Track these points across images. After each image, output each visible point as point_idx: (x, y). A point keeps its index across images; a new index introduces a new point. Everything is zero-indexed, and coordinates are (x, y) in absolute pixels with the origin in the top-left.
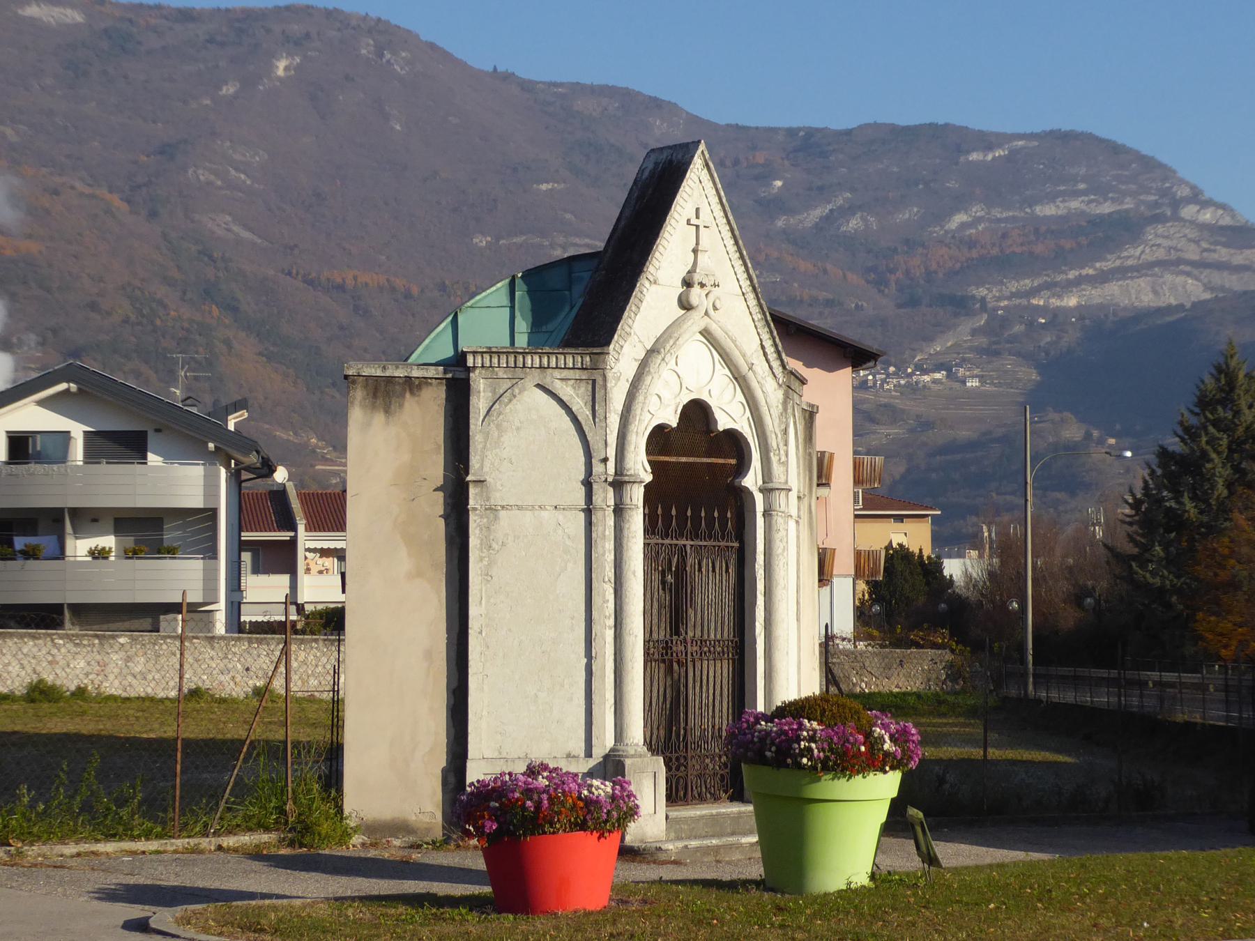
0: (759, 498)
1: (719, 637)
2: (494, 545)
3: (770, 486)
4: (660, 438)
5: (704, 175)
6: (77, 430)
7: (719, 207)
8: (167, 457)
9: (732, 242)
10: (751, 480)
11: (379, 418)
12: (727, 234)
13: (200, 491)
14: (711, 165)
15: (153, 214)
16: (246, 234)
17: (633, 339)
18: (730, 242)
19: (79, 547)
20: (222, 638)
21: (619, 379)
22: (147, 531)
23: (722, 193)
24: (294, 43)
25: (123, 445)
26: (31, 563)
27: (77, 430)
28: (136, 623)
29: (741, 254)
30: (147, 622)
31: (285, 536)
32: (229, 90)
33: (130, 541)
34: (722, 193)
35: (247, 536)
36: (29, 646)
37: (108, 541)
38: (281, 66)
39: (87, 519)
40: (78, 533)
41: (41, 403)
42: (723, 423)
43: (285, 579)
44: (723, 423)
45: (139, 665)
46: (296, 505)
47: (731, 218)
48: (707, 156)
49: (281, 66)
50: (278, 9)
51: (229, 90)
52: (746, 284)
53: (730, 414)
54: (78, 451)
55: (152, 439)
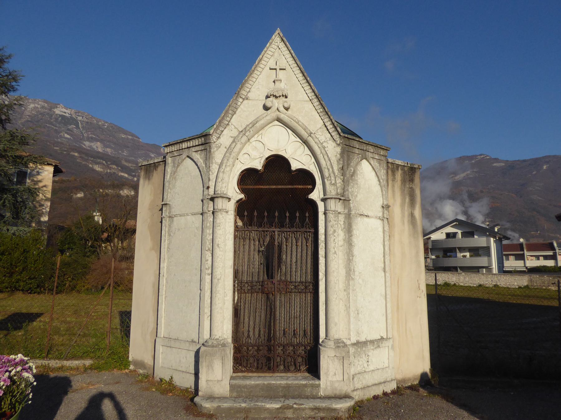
0: (321, 206)
1: (304, 280)
2: (172, 234)
3: (326, 197)
4: (248, 177)
5: (282, 45)
6: (459, 232)
7: (292, 59)
8: (479, 236)
9: (301, 75)
10: (316, 195)
11: (147, 182)
12: (297, 71)
13: (485, 243)
14: (284, 39)
15: (521, 197)
16: (540, 198)
17: (231, 127)
18: (300, 75)
19: (460, 255)
20: (495, 274)
21: (220, 147)
22: (475, 251)
23: (292, 52)
24: (547, 163)
25: (468, 234)
26: (450, 258)
27: (459, 232)
28: (474, 271)
29: (307, 80)
30: (477, 270)
31: (522, 252)
32: (534, 173)
33: (472, 254)
34: (292, 52)
35: (504, 253)
36: (443, 275)
37: (468, 254)
38: (545, 167)
39: (462, 249)
40: (461, 252)
41: (451, 227)
42: (295, 166)
43: (522, 262)
44: (295, 166)
45: (467, 279)
46: (524, 246)
47: (299, 63)
48: (282, 35)
49: (545, 167)
50: (543, 157)
51: (534, 173)
52: (311, 95)
53: (299, 159)
54: (459, 236)
55: (475, 233)
